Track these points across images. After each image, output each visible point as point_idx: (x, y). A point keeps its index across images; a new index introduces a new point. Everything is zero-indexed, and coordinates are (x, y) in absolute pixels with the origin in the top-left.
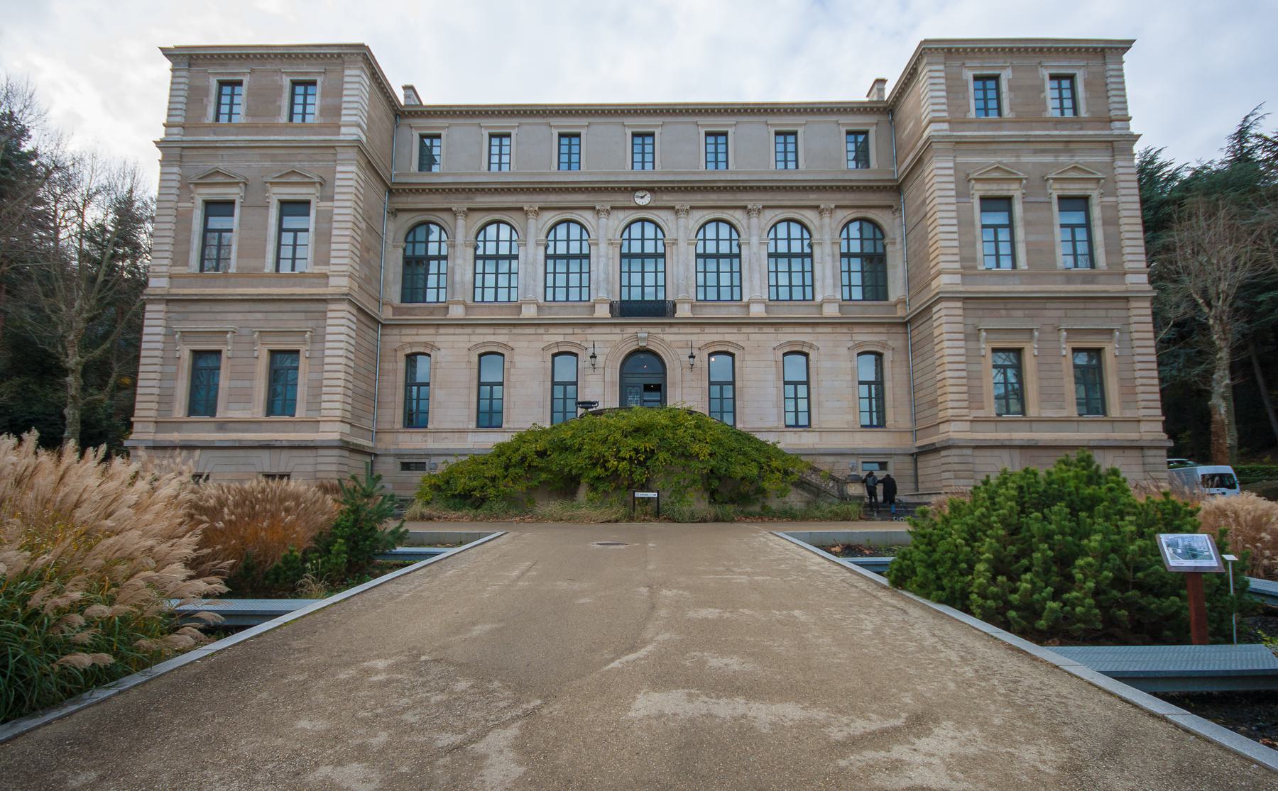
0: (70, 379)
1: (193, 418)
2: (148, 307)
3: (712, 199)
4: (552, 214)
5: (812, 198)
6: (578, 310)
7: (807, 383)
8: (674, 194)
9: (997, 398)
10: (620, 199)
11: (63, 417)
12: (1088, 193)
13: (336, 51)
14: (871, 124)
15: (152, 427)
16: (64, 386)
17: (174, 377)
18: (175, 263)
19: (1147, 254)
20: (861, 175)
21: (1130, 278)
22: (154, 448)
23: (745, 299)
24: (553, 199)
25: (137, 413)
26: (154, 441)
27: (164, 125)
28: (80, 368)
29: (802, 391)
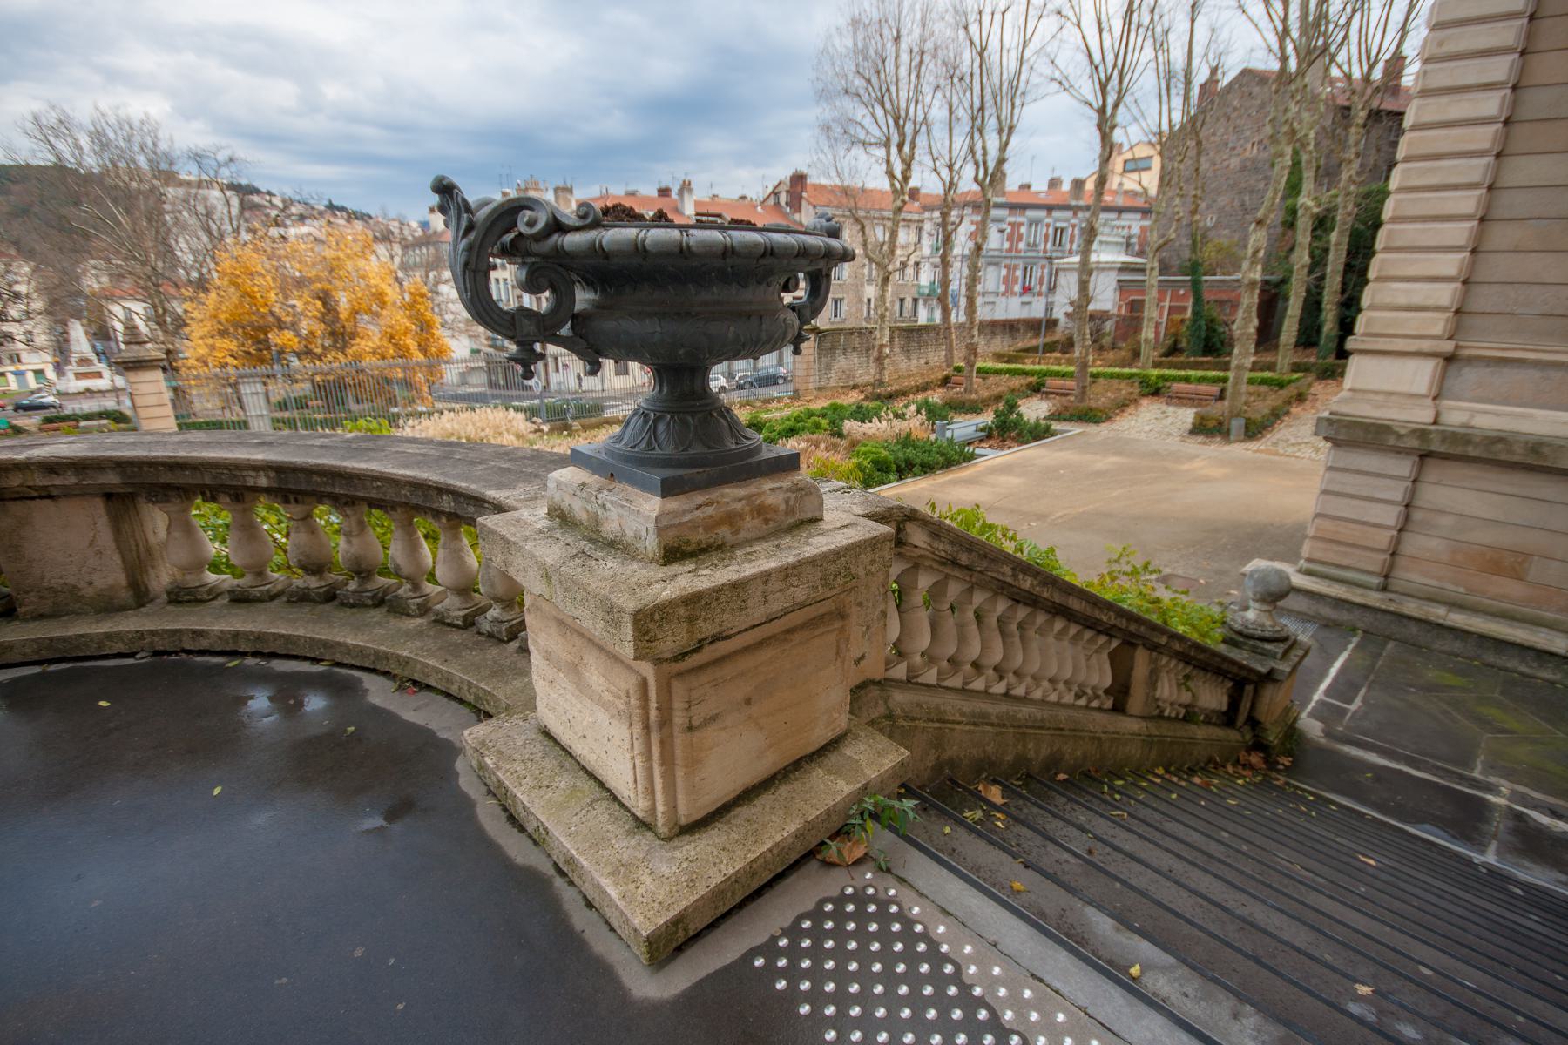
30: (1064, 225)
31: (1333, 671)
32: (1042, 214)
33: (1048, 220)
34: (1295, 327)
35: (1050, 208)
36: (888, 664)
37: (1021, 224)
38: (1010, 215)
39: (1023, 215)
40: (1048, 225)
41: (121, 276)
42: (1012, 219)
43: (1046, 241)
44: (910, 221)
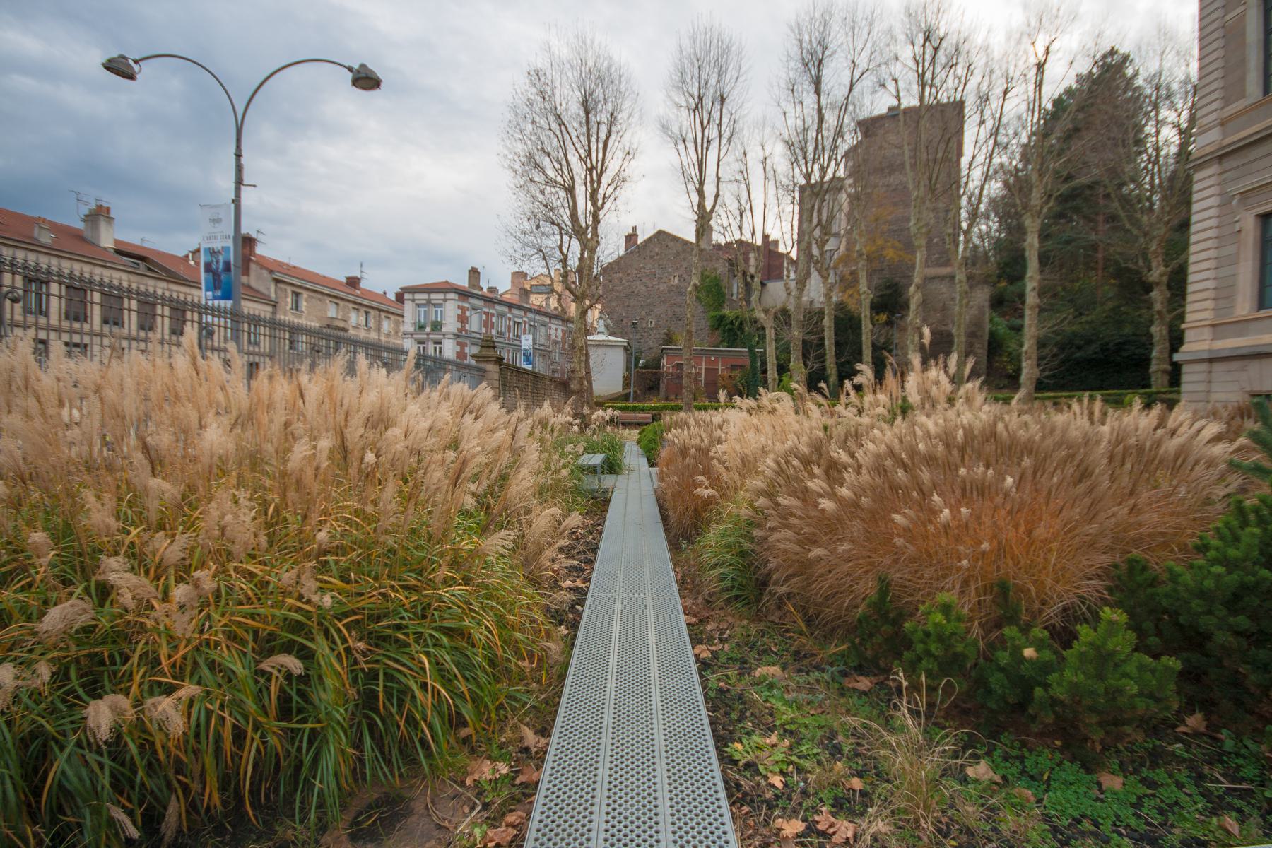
0: (1155, 294)
1: (1264, 313)
2: (1197, 177)
11: (1151, 336)
13: (89, 314)
15: (1207, 333)
16: (1150, 306)
17: (1234, 260)
18: (1227, 101)
22: (1211, 360)
25: (1189, 317)
26: (1210, 351)
27: (907, 9)
28: (1165, 279)
30: (520, 321)
31: (653, 649)
32: (505, 309)
33: (509, 315)
34: (1228, 341)
35: (511, 306)
36: (493, 773)
37: (493, 315)
38: (485, 306)
39: (493, 308)
40: (510, 319)
41: (748, 765)
42: (486, 310)
43: (509, 332)
44: (360, 304)
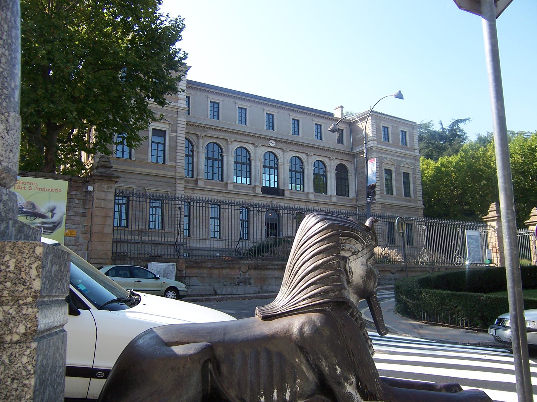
3: (296, 148)
4: (237, 143)
5: (328, 154)
6: (302, 195)
7: (219, 219)
8: (283, 144)
9: (33, 206)
10: (264, 142)
12: (410, 172)
14: (344, 128)
19: (423, 194)
20: (340, 147)
21: (419, 202)
23: (253, 185)
24: (239, 137)
29: (217, 221)
